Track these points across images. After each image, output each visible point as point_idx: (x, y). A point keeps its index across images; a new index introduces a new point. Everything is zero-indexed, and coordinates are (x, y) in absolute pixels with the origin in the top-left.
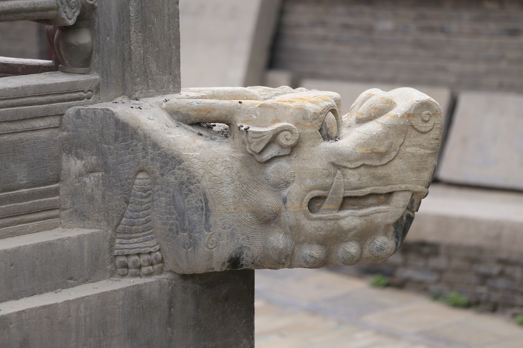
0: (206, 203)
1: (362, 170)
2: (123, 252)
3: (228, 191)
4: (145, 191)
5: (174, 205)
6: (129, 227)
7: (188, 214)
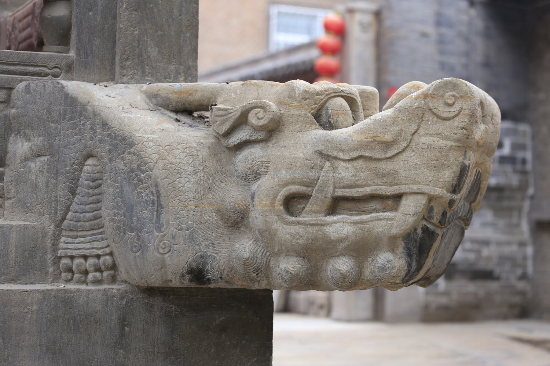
0: (159, 196)
1: (360, 163)
3: (188, 183)
4: (94, 181)
6: (75, 223)
7: (136, 209)
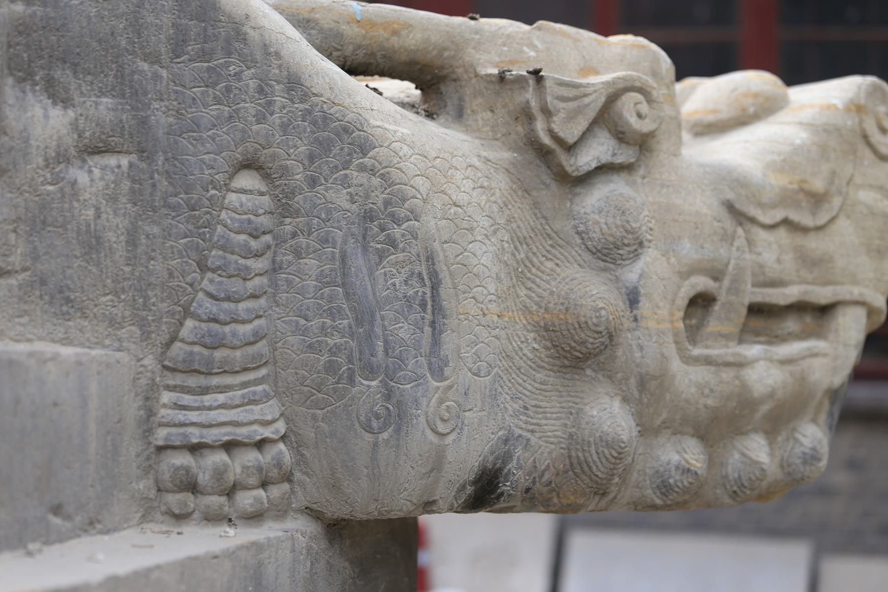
0: (435, 287)
2: (184, 435)
5: (343, 285)
6: (206, 352)
